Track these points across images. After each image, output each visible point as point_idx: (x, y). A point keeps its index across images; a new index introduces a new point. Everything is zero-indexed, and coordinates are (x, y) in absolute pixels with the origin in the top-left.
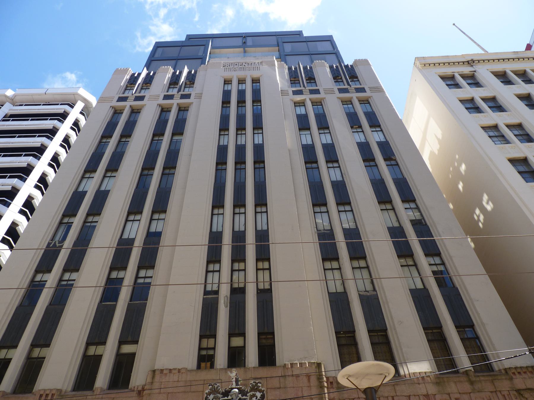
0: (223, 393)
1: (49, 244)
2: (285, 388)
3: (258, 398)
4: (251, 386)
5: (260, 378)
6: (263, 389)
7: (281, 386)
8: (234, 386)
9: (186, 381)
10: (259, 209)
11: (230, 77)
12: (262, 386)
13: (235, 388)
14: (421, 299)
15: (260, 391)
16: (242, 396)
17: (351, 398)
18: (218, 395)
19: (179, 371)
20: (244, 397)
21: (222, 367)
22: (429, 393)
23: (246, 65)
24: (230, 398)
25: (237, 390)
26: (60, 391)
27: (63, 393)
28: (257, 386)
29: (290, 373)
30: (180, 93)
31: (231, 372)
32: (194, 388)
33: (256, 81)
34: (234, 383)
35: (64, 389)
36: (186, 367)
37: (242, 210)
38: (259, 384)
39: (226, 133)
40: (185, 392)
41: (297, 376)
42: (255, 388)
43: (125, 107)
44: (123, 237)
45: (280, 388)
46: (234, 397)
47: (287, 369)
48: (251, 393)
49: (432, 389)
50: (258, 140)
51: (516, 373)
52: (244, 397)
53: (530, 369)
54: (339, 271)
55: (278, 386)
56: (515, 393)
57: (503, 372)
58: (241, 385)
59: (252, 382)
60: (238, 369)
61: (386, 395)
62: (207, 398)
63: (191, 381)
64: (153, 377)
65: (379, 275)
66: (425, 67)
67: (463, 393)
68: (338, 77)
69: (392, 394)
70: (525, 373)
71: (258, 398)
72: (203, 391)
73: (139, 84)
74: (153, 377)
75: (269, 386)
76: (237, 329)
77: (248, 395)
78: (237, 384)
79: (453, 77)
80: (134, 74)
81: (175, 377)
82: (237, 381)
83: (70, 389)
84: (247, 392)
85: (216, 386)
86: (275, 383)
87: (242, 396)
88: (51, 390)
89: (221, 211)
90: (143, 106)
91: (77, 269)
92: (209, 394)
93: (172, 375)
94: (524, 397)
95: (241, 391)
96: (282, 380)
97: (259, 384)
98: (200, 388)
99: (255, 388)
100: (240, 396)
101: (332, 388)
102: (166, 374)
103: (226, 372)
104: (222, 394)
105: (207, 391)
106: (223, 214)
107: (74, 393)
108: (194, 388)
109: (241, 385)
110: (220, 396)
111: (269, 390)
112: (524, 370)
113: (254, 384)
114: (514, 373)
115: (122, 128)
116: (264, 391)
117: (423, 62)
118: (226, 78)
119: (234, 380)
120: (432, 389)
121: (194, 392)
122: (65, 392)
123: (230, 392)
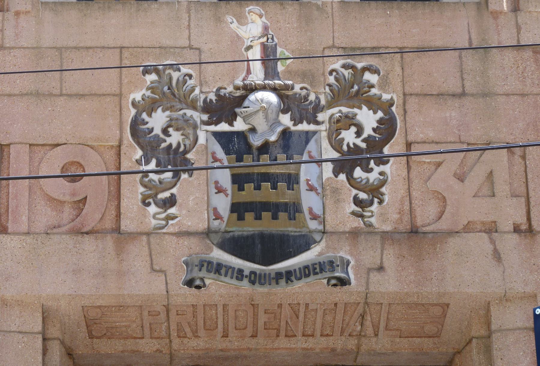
0: (207, 108)
2: (486, 95)
3: (368, 131)
4: (331, 79)
5: (375, 52)
6: (386, 97)
7: (469, 87)
8: (257, 74)
9: (37, 50)
12: (384, 84)
13: (264, 88)
15: (374, 104)
16: (297, 121)
18: (189, 112)
20: (304, 127)
25: (271, 98)
28: (360, 82)
29: (507, 37)
31: (242, 20)
32: (75, 82)
34: (257, 68)
38: (367, 76)
40: (37, 94)
42: (351, 91)
45: (463, 94)
46: (260, 123)
47: (496, 15)
52: (304, 127)
54: (117, 99)
55: (453, 85)
57: (223, 271)
59: (337, 65)
60: (273, 7)
63: (59, 49)
65: (248, 58)
71: (368, 131)
72: (120, 96)
75: (416, 86)
77: (321, 117)
82: (269, 59)
84: (318, 108)
85: (175, 75)
86: (441, 72)
87: (297, 121)
92: (150, 107)
95: (288, 101)
96: (471, 61)
98: (107, 81)
99: (351, 91)
100: (286, 120)
103: (219, 20)
105: (138, 96)
108: (75, 82)
109: (289, 73)
110: (197, 116)
111: (412, 103)
113: (347, 73)
119: (256, 53)
121: (81, 96)
123: (240, 101)
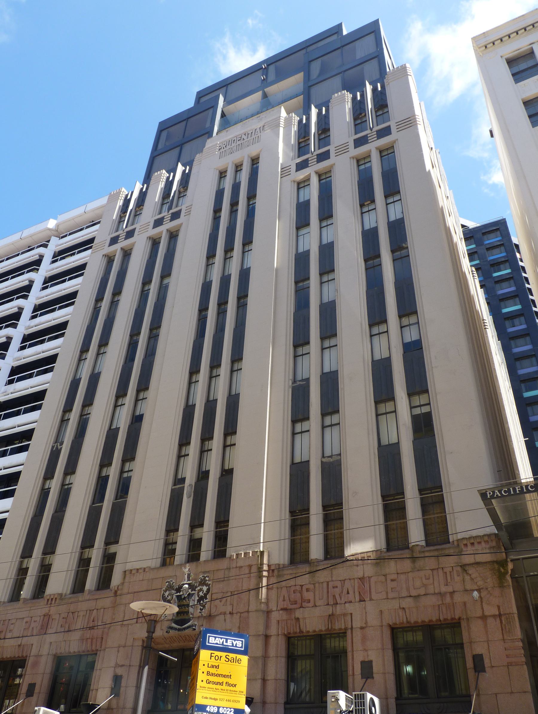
1: (53, 447)
10: (405, 321)
11: (241, 160)
13: (186, 584)
14: (388, 458)
15: (207, 585)
16: (192, 591)
17: (288, 586)
19: (144, 569)
20: (193, 592)
21: (178, 563)
22: (365, 576)
23: (245, 137)
24: (181, 593)
26: (61, 595)
27: (281, 566)
30: (171, 211)
33: (255, 161)
35: (282, 563)
36: (150, 566)
37: (413, 319)
38: (207, 579)
39: (396, 198)
41: (241, 567)
43: (161, 233)
44: (112, 428)
48: (199, 588)
49: (369, 570)
50: (395, 213)
51: (469, 545)
52: (193, 592)
53: (486, 538)
56: (459, 569)
58: (192, 580)
61: (322, 580)
62: (164, 594)
64: (124, 578)
66: (488, 50)
67: (402, 573)
68: (361, 114)
69: (327, 580)
70: (479, 543)
71: (205, 592)
73: (131, 210)
74: (124, 578)
76: (197, 522)
78: (189, 580)
79: (45, 246)
80: (127, 195)
81: (140, 576)
82: (189, 576)
83: (69, 592)
84: (196, 587)
87: (192, 591)
88: (54, 595)
89: (383, 328)
90: (133, 244)
91: (73, 472)
92: (165, 591)
93: (138, 574)
94: (467, 573)
97: (207, 579)
99: (203, 582)
101: (273, 576)
102: (134, 574)
103: (181, 568)
104: (176, 590)
106: (387, 332)
107: (71, 595)
109: (192, 580)
112: (479, 540)
114: (466, 545)
115: (161, 266)
116: (210, 584)
117: (483, 42)
118: (220, 169)
120: (369, 570)
122: (65, 595)
